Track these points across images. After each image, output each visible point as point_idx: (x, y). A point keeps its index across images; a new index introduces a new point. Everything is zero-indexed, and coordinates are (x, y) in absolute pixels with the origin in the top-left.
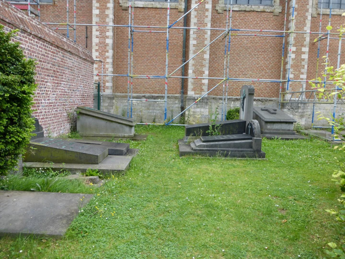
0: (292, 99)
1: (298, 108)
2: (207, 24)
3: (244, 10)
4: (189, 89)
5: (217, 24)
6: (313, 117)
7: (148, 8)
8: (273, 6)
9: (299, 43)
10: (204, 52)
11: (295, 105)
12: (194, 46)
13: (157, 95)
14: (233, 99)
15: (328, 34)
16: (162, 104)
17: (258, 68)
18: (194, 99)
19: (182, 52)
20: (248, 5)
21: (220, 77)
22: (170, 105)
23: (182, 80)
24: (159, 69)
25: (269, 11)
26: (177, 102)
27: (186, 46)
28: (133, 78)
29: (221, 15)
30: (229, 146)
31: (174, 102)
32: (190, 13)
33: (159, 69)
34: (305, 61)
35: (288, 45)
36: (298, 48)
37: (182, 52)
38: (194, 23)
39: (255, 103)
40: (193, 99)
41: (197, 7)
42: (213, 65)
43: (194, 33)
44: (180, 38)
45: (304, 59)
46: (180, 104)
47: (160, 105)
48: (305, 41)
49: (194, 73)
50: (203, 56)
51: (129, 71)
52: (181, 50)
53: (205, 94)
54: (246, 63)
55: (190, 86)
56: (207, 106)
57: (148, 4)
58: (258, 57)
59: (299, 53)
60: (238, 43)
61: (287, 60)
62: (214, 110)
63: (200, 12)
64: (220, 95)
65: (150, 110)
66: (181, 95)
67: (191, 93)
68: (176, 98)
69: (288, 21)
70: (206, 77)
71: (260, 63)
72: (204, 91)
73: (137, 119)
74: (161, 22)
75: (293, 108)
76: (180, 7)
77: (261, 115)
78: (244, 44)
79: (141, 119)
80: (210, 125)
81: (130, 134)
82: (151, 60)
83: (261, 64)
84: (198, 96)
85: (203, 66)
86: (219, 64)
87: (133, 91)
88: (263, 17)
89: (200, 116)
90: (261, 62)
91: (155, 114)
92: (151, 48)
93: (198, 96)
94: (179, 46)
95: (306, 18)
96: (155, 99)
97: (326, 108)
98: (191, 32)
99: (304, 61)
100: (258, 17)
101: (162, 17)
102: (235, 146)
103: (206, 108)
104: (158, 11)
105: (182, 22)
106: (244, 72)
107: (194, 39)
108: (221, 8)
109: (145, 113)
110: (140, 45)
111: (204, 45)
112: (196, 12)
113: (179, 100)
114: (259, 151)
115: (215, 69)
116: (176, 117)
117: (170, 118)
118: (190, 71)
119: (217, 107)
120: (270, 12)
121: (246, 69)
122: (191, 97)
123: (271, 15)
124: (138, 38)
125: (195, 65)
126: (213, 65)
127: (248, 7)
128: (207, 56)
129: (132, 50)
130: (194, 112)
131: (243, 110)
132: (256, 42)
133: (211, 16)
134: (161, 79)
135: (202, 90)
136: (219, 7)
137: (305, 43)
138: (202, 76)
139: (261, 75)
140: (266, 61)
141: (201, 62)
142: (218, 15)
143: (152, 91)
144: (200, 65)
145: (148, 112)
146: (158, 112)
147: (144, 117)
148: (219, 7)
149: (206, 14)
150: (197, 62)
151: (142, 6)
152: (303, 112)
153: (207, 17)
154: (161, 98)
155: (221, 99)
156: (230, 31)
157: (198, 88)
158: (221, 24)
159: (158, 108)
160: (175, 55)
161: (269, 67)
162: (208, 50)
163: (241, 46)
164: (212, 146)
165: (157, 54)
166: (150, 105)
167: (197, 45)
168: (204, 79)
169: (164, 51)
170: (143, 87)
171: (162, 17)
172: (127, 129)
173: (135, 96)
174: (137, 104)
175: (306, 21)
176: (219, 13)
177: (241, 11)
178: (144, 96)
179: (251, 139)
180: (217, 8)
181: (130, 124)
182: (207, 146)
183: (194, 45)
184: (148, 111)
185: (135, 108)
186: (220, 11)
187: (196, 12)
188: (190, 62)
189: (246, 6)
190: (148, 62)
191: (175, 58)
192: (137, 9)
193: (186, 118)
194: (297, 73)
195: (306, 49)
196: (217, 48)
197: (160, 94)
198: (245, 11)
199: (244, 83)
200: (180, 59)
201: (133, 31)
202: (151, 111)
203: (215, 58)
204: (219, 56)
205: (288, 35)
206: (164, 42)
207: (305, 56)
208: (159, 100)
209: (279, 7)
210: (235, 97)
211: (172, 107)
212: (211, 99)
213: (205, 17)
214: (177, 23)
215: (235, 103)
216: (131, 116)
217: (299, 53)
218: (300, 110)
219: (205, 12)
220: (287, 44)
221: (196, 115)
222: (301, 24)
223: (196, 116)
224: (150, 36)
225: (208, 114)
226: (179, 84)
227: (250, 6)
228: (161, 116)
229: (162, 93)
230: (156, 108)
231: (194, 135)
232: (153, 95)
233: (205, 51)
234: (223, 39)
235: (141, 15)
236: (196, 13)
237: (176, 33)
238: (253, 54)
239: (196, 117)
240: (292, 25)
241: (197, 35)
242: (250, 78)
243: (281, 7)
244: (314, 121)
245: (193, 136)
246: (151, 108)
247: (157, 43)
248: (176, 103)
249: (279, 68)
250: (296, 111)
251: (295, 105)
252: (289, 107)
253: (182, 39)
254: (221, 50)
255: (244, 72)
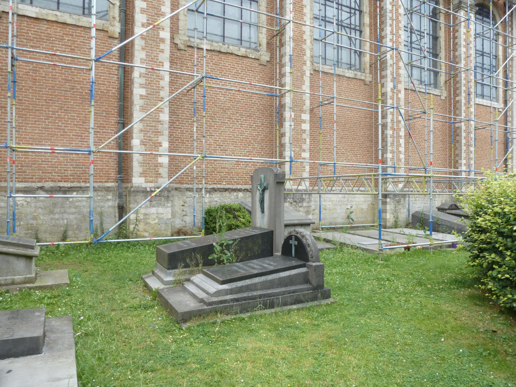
0: (299, 188)
1: (302, 200)
2: (163, 63)
3: (218, 50)
4: (134, 174)
5: (176, 65)
6: (320, 212)
7: (48, 21)
8: (259, 51)
9: (298, 107)
10: (160, 110)
11: (298, 196)
12: (142, 99)
13: (69, 185)
14: (208, 190)
15: (333, 98)
16: (80, 201)
17: (242, 140)
18: (146, 192)
19: (117, 107)
20: (223, 44)
21: (185, 153)
22: (98, 204)
23: (119, 158)
24: (73, 135)
25: (253, 57)
26: (110, 197)
27: (124, 97)
28: (16, 151)
29: (183, 52)
30: (272, 284)
31: (105, 197)
32: (132, 42)
33: (73, 135)
34: (306, 132)
35: (283, 108)
36: (297, 114)
37: (117, 107)
38: (141, 59)
39: (242, 195)
40: (143, 192)
41: (145, 34)
42: (174, 132)
43: (140, 76)
44: (113, 82)
45: (305, 130)
46: (115, 201)
47: (77, 204)
48: (305, 104)
49: (143, 144)
50: (159, 116)
51: (9, 138)
52: (115, 103)
53: (164, 182)
54: (225, 132)
55: (136, 167)
56: (168, 203)
57: (47, 15)
58: (242, 124)
59: (297, 121)
60: (212, 100)
61: (282, 130)
62: (178, 209)
63: (151, 42)
64: (186, 183)
65: (54, 214)
66: (117, 184)
67: (138, 180)
68: (108, 189)
69: (282, 75)
70: (165, 152)
71: (245, 134)
72: (162, 177)
73: (27, 234)
74: (74, 50)
75: (295, 202)
76: (111, 29)
77: (256, 216)
78: (220, 103)
79: (36, 234)
80: (214, 244)
81: (29, 276)
82: (55, 118)
83: (246, 135)
84: (152, 185)
85: (158, 133)
86: (183, 131)
87: (16, 178)
88: (246, 65)
89: (156, 221)
90: (246, 131)
91: (65, 221)
92: (56, 96)
93: (152, 185)
94: (111, 96)
95: (303, 74)
96: (65, 194)
97: (332, 199)
98: (136, 74)
99: (305, 133)
100: (238, 64)
101: (77, 41)
102: (282, 283)
103: (168, 207)
104: (68, 29)
105: (115, 56)
106: (222, 146)
107: (141, 86)
108: (182, 42)
109: (44, 220)
110: (30, 87)
111: (159, 98)
112: (144, 41)
113: (113, 193)
114: (320, 286)
115: (176, 140)
116: (112, 226)
117: (97, 227)
118: (136, 142)
119: (183, 204)
120: (254, 59)
121: (225, 141)
122: (138, 187)
123: (256, 64)
124: (27, 73)
125: (144, 131)
126: (174, 132)
127: (224, 46)
128: (165, 117)
129: (14, 97)
130: (145, 214)
131: (263, 211)
132: (238, 101)
133: (169, 51)
134: (76, 154)
135: (158, 175)
136: (180, 39)
137: (305, 108)
138: (158, 151)
139: (247, 152)
140: (254, 130)
141: (156, 127)
142: (178, 52)
143: (59, 178)
144: (153, 132)
145: (52, 219)
146: (72, 217)
147: (43, 228)
148: (180, 39)
149: (161, 47)
150: (147, 126)
151: (34, 16)
152: (308, 207)
153: (162, 51)
154: (77, 191)
155: (188, 190)
156: (205, 79)
157: (152, 172)
158: (183, 67)
159: (73, 210)
160: (103, 111)
161: (257, 139)
162: (166, 107)
163: (217, 106)
164: (240, 290)
165: (68, 107)
166: (55, 205)
167: (147, 97)
168: (161, 155)
169: (82, 103)
170: (38, 170)
171: (77, 41)
172: (21, 264)
173: (22, 188)
174: (25, 203)
175: (305, 78)
176: (179, 50)
177: (214, 51)
178: (42, 188)
179: (304, 266)
180: (177, 41)
181: (29, 252)
182: (231, 292)
183: (141, 96)
184: (51, 216)
185: (21, 213)
186: (182, 47)
187: (144, 41)
188: (135, 126)
189: (221, 44)
190: (49, 122)
191: (105, 116)
192: (22, 19)
193: (132, 227)
194: (298, 149)
195: (306, 117)
196: (179, 106)
197: (75, 183)
198: (219, 52)
199: (223, 164)
200: (114, 119)
201: (17, 60)
202: (57, 216)
203: (176, 120)
204: (182, 118)
205: (282, 96)
206: (81, 87)
207: (306, 126)
208: (74, 194)
209: (266, 54)
210: (211, 186)
211: (102, 207)
212: (172, 190)
213: (159, 51)
214: (109, 55)
215: (211, 196)
216: (14, 228)
217: (297, 121)
218: (305, 204)
219: (159, 43)
220: (282, 107)
221: (149, 219)
222: (298, 81)
223: (150, 221)
224: (52, 72)
225: (170, 217)
226: (113, 164)
227: (226, 46)
228: (78, 226)
229: (79, 182)
230: (68, 211)
231: (187, 266)
232: (61, 184)
233: (161, 109)
234: (188, 92)
235: (31, 31)
236: (143, 43)
237: (105, 73)
238: (235, 119)
239: (149, 223)
240: (288, 80)
241: (146, 80)
242: (232, 156)
243: (268, 53)
244: (322, 217)
245: (185, 267)
246: (57, 210)
247: (67, 88)
248: (108, 200)
249: (273, 143)
250: (300, 205)
251: (298, 196)
252: (291, 200)
253: (116, 85)
254: (184, 109)
255: (222, 146)
